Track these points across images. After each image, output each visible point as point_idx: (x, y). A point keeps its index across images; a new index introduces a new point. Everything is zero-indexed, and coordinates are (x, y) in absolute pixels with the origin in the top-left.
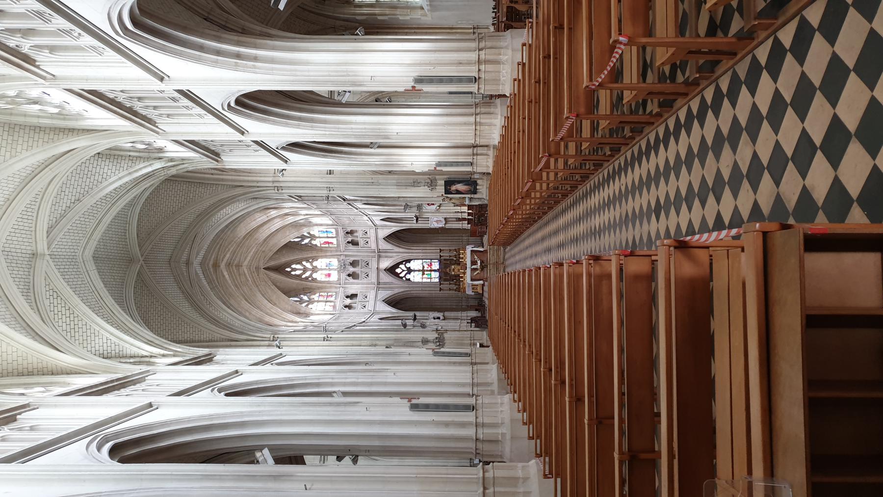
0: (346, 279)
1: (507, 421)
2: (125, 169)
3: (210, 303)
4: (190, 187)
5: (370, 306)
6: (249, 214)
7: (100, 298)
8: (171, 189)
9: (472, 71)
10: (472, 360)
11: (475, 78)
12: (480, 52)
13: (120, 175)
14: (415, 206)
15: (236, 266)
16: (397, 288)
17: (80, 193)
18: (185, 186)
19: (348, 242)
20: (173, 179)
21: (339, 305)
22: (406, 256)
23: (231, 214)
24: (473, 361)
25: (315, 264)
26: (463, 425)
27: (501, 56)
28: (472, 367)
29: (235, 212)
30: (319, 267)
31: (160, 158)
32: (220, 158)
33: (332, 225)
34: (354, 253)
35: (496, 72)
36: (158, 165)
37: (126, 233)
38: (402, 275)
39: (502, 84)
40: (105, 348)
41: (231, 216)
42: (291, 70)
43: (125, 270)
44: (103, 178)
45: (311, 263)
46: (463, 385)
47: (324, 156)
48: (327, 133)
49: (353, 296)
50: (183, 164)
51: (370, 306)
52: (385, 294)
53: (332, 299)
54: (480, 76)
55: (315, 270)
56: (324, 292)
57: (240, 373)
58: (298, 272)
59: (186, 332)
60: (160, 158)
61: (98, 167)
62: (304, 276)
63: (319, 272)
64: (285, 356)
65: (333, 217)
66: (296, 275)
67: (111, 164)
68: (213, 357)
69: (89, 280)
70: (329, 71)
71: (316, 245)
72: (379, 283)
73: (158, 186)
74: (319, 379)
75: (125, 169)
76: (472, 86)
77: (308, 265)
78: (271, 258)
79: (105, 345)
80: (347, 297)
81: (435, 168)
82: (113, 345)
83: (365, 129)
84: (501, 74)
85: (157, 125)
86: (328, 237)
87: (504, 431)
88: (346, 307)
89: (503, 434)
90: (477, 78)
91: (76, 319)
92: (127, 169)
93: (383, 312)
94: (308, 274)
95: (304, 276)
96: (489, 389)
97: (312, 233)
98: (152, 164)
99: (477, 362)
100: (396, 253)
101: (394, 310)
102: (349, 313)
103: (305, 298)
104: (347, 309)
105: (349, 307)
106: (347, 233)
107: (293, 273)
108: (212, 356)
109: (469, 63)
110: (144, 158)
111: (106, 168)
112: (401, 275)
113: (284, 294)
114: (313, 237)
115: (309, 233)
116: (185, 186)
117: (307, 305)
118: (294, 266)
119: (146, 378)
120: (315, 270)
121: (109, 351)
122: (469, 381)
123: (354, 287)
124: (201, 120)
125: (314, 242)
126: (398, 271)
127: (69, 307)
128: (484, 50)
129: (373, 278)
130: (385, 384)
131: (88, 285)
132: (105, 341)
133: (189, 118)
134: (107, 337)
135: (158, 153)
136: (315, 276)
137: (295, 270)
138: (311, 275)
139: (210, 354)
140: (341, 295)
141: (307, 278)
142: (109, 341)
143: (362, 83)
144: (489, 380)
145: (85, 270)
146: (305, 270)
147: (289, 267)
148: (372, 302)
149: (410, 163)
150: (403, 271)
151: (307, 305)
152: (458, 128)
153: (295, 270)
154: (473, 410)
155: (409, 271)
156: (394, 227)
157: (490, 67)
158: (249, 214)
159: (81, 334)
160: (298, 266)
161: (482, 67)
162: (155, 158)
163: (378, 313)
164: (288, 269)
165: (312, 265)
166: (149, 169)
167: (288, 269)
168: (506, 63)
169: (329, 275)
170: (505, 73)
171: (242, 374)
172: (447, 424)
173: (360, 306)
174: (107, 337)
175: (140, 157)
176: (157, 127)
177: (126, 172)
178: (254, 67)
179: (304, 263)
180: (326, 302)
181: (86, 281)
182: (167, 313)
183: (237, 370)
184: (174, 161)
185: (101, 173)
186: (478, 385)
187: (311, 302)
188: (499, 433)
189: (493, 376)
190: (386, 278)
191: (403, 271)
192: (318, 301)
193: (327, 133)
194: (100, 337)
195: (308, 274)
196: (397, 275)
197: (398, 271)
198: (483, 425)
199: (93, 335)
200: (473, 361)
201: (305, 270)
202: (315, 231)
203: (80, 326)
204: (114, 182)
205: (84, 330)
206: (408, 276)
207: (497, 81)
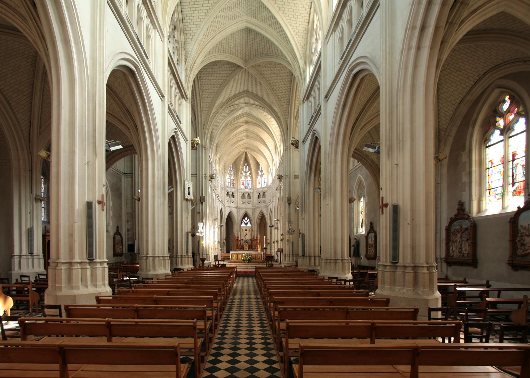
0: (241, 193)
1: (76, 292)
2: (299, 41)
3: (226, 117)
4: (287, 99)
5: (228, 204)
6: (272, 137)
7: (220, 31)
8: (286, 87)
9: (404, 257)
10: (184, 255)
11: (397, 263)
12: (426, 268)
13: (295, 38)
14: (277, 225)
15: (247, 130)
16: (237, 217)
17: (284, 11)
18: (287, 95)
19: (259, 193)
20: (293, 77)
21: (229, 190)
22: (253, 222)
23: (272, 127)
24: (183, 256)
25: (249, 177)
26: (71, 250)
27: (422, 288)
28: (167, 257)
29: (273, 129)
30: (247, 179)
31: (305, 64)
32: (306, 101)
33: (268, 185)
34: (255, 196)
35: (404, 283)
36: (301, 63)
37: (261, 55)
38: (244, 220)
39: (390, 288)
40: (189, 32)
41: (271, 127)
42: (404, 86)
43: (240, 56)
44: (293, 26)
45: (249, 176)
46: (154, 250)
47: (308, 164)
48: (327, 156)
49: (233, 196)
50: (302, 79)
51: (228, 204)
52: (234, 212)
53: (232, 186)
54: (398, 268)
55: (246, 177)
56: (235, 182)
57: (162, 99)
58: (245, 169)
59: (208, 98)
60: (305, 64)
61: (300, 23)
62: (243, 172)
63: (245, 179)
64: (186, 143)
65: (272, 185)
66: (243, 168)
67: (302, 31)
68: (185, 99)
69: (231, 24)
70: (403, 123)
71: (258, 178)
72: (239, 209)
73: (287, 68)
74: (157, 151)
75: (299, 41)
76: (388, 258)
77: (248, 174)
78: (251, 155)
79: (191, 32)
80: (233, 193)
81: (301, 233)
82: (191, 37)
83: (331, 182)
84: (402, 287)
85: (333, 32)
86: (262, 183)
87: (64, 290)
88: (228, 192)
89: (60, 289)
90: (398, 265)
91: (206, 11)
92: (299, 43)
93: (225, 211)
94: (244, 174)
95: (243, 172)
96: (151, 268)
97: (264, 175)
98: (302, 59)
99: (183, 259)
100: (256, 217)
101: (226, 216)
102: (225, 194)
103: (232, 173)
104: (227, 193)
105: (228, 194)
106: (264, 193)
107: (244, 167)
108: (186, 99)
109: (413, 257)
110: (306, 54)
111: (300, 28)
112: (244, 220)
113: (234, 162)
114: (262, 176)
115: (264, 174)
116: (287, 95)
117: (229, 174)
118: (248, 167)
119: (156, 30)
120: (246, 177)
121: (188, 35)
122: (157, 255)
123: (238, 196)
124: (337, 63)
125: (259, 176)
126: (246, 219)
127: (213, 6)
128: (428, 272)
129: (243, 206)
130: (154, 197)
131: (228, 24)
132: (194, 31)
133: (339, 54)
134: (196, 33)
135: (309, 62)
136: (243, 177)
137: (246, 168)
138: (244, 176)
139: (187, 98)
140: (233, 190)
141: (242, 174)
142: (193, 34)
143: (390, 157)
144: (157, 268)
145: (237, 21)
146: (246, 172)
147: (247, 165)
148: (230, 205)
149: (304, 218)
150: (246, 221)
151: (229, 174)
152: (333, 247)
153: (246, 168)
154: (89, 259)
155: (246, 224)
156: (267, 216)
157: (409, 277)
158: (272, 137)
159: (198, 15)
160: (247, 169)
161: (409, 270)
162: (305, 61)
163: (224, 208)
164: (246, 165)
165: (248, 176)
166: (298, 57)
167: (246, 165)
168: (414, 292)
169: (243, 184)
170: (402, 291)
171: (161, 100)
172: (71, 235)
173: (228, 199)
174: (196, 33)
175: (306, 51)
176: (332, 33)
177: (297, 42)
178: (409, 49)
179: (249, 172)
180: (230, 183)
181: (230, 22)
182: (218, 87)
183: (164, 97)
184: (303, 73)
185: (296, 25)
186: (154, 261)
187: (230, 175)
188: (62, 284)
189: (161, 271)
190: (242, 213)
191: (246, 221)
192: (230, 179)
193: (327, 156)
194: (196, 29)
195: (244, 174)
196: (244, 218)
197: (246, 219)
198: (70, 270)
199: (197, 23)
200: (183, 257)
201: (246, 172)
202: (265, 176)
203: (202, 14)
204: (291, 34)
205: (200, 17)
206: (243, 223)
207: (393, 282)
